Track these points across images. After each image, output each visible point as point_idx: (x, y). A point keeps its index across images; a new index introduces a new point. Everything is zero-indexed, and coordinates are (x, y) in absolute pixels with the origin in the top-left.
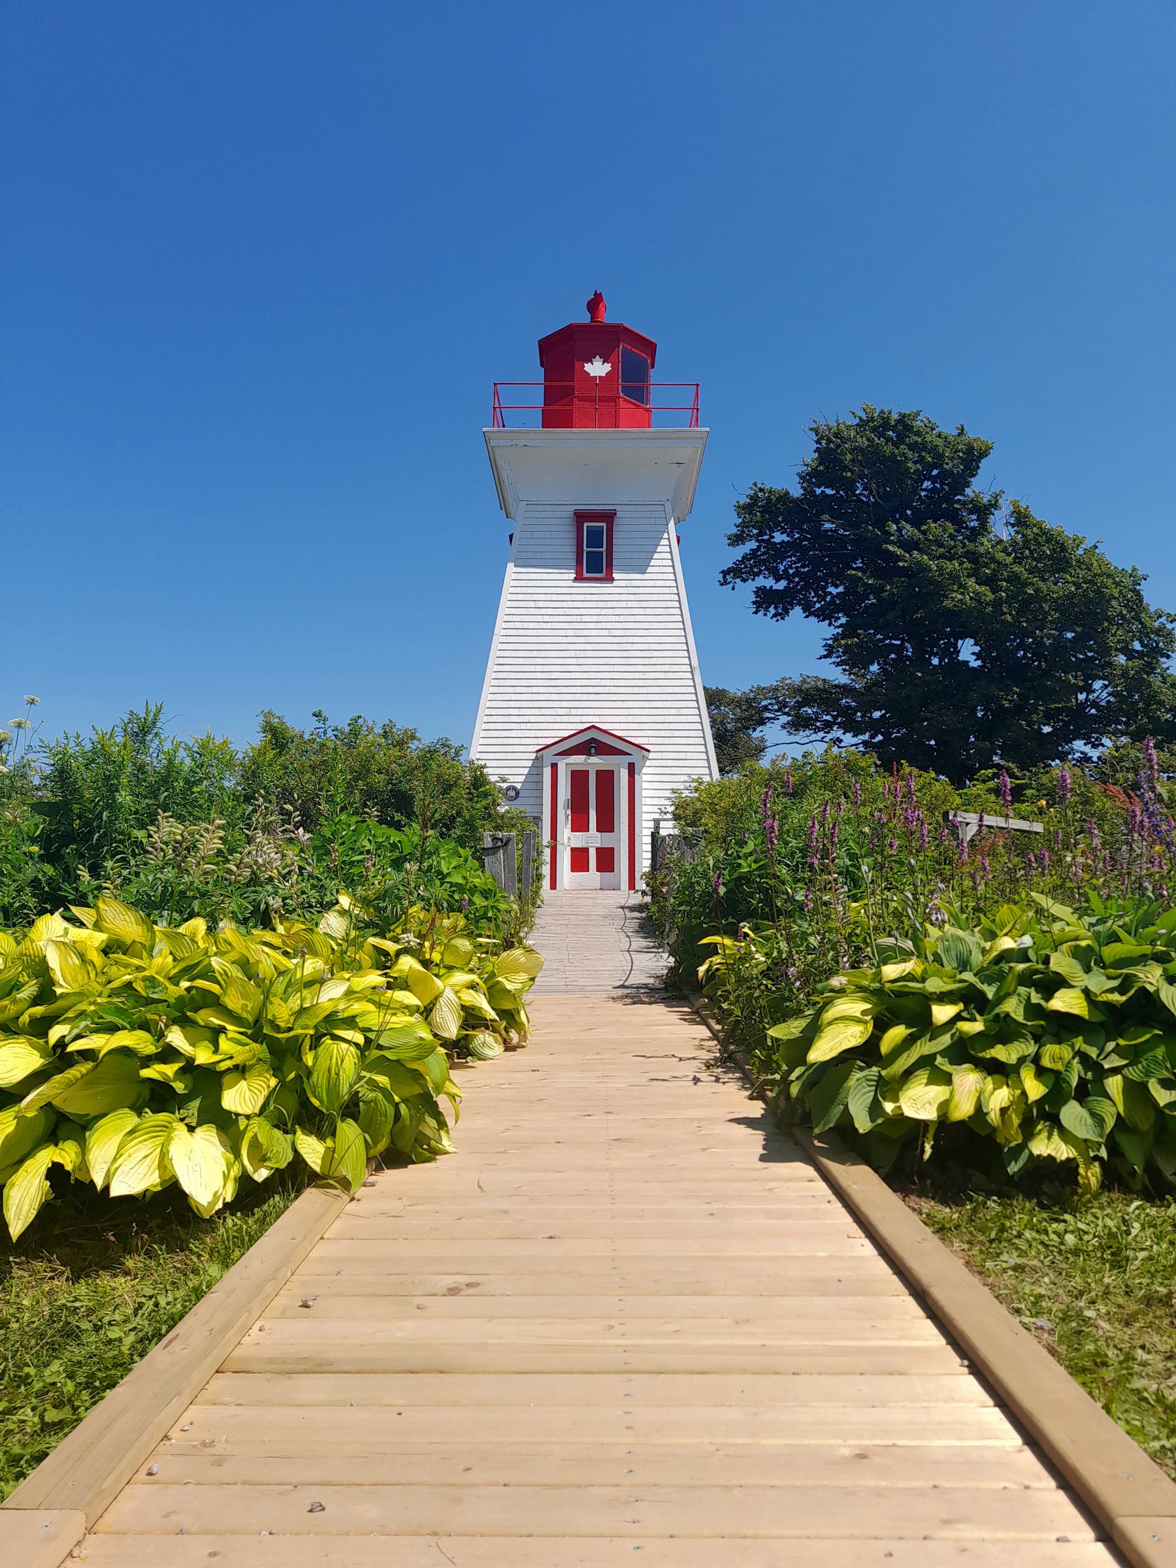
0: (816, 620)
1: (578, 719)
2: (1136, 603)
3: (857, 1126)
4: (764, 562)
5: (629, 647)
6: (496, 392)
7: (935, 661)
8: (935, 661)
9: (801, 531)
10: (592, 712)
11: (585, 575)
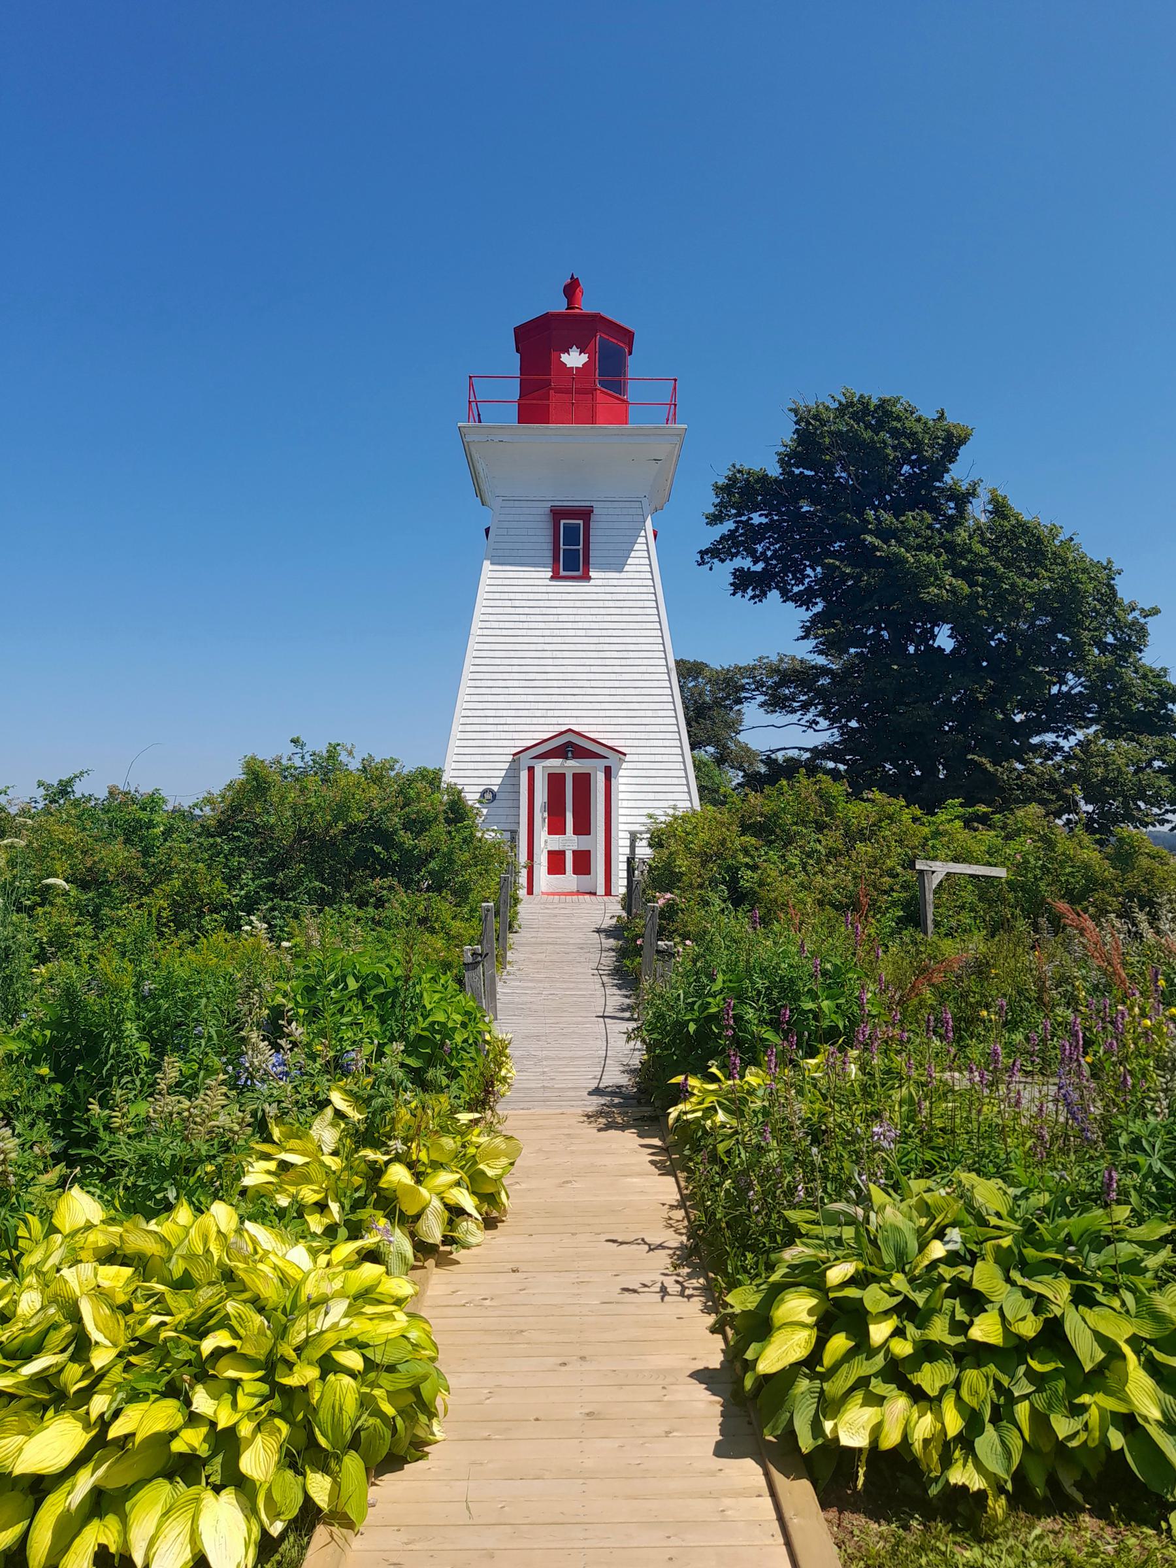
0: (793, 605)
1: (554, 721)
2: (1110, 598)
3: (801, 1445)
4: (742, 543)
5: (606, 647)
6: (471, 385)
7: (911, 649)
8: (911, 649)
9: (780, 513)
10: (568, 713)
11: (562, 573)
